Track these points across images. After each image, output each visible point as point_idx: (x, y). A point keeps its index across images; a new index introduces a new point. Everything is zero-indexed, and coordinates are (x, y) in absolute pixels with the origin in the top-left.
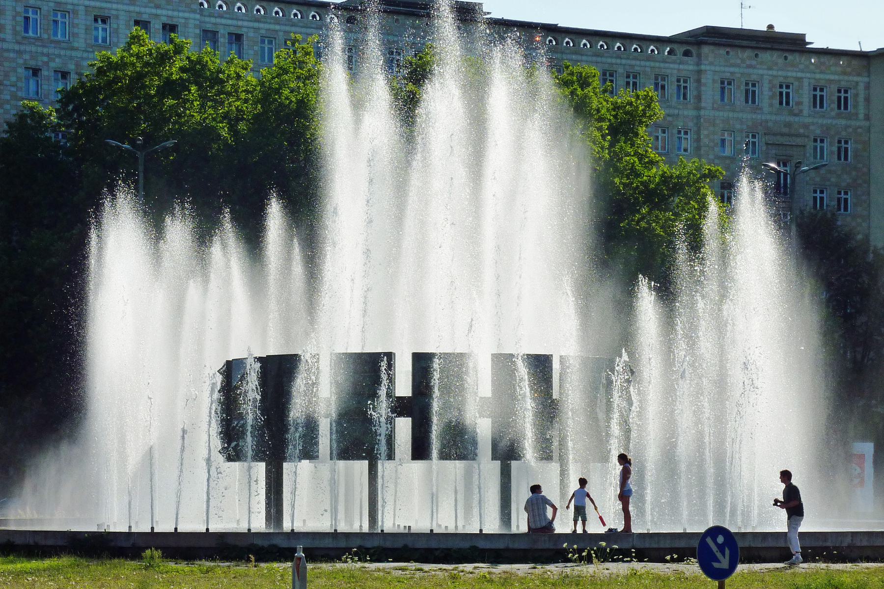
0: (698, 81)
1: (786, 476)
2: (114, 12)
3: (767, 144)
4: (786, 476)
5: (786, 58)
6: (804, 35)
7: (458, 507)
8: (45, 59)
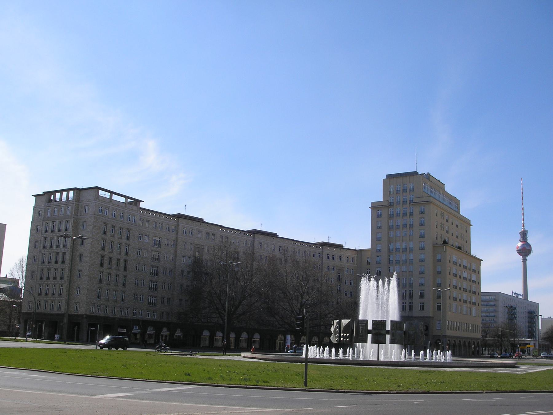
0: (322, 254)
1: (6, 275)
2: (202, 230)
3: (336, 269)
4: (6, 275)
5: (340, 250)
6: (276, 234)
7: (206, 355)
8: (187, 240)
